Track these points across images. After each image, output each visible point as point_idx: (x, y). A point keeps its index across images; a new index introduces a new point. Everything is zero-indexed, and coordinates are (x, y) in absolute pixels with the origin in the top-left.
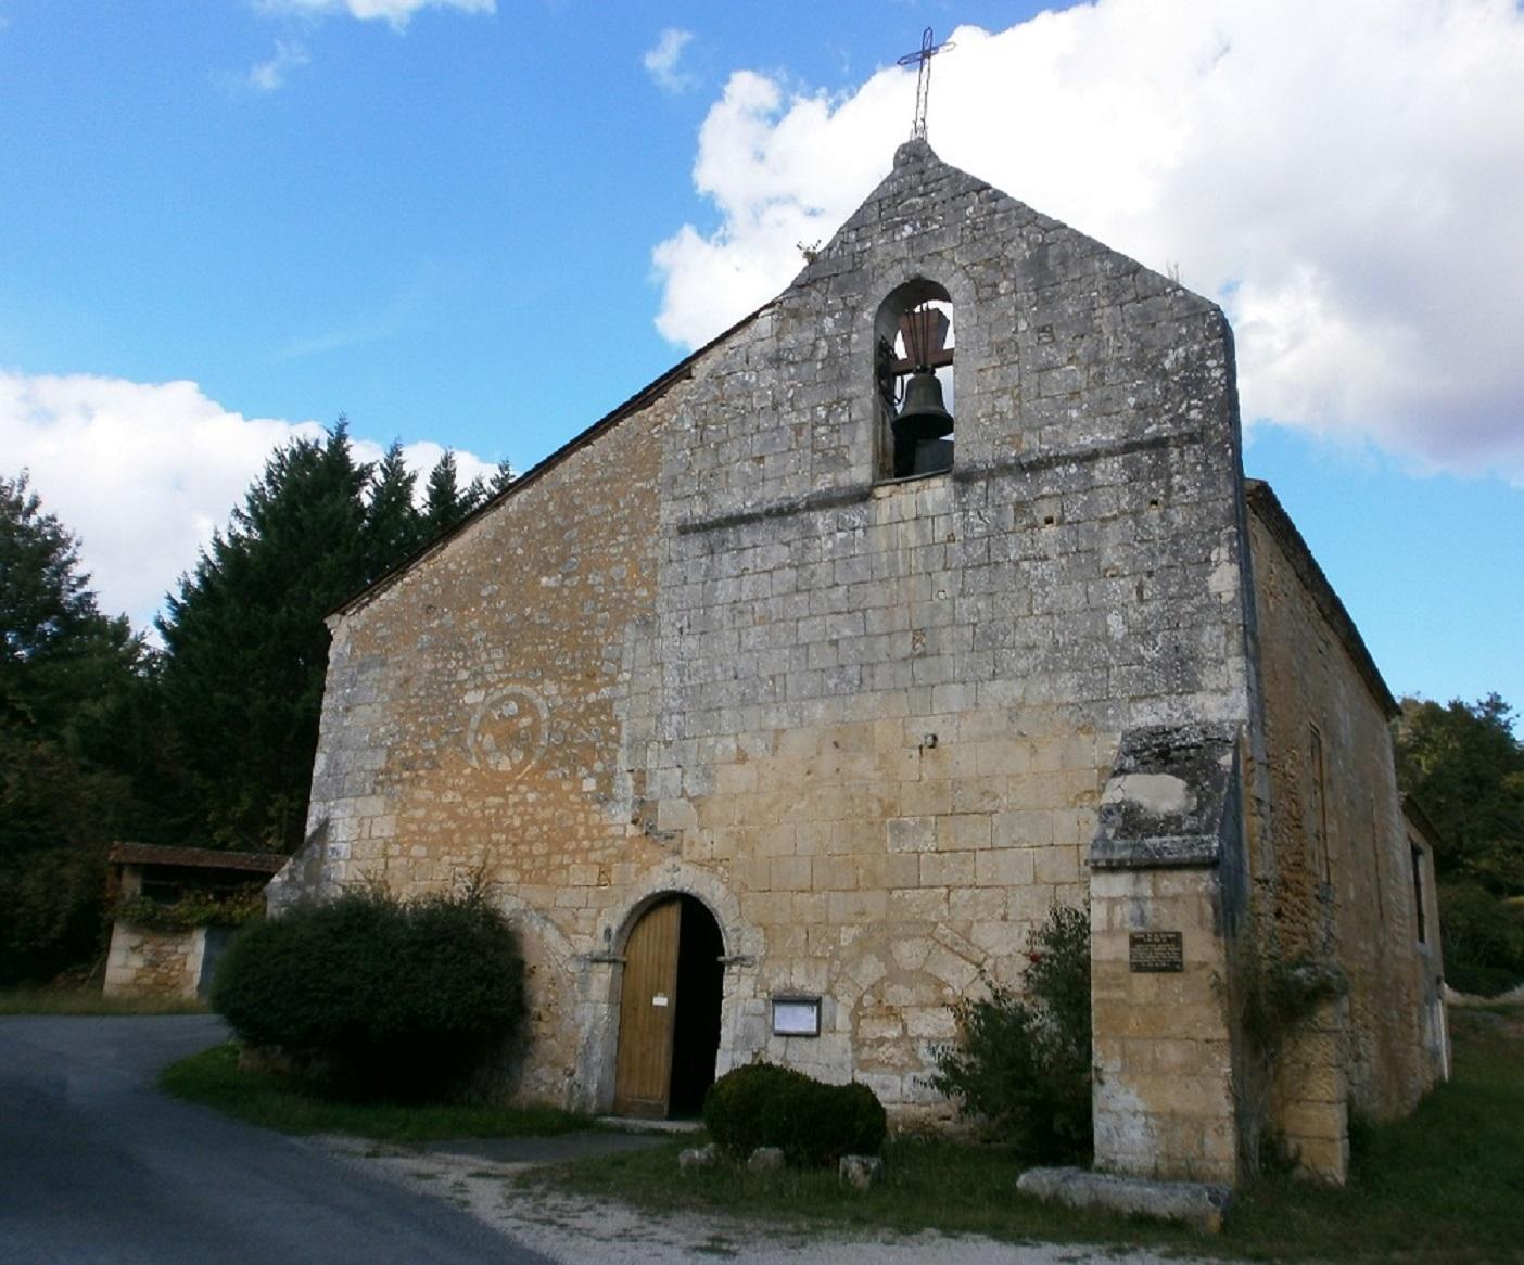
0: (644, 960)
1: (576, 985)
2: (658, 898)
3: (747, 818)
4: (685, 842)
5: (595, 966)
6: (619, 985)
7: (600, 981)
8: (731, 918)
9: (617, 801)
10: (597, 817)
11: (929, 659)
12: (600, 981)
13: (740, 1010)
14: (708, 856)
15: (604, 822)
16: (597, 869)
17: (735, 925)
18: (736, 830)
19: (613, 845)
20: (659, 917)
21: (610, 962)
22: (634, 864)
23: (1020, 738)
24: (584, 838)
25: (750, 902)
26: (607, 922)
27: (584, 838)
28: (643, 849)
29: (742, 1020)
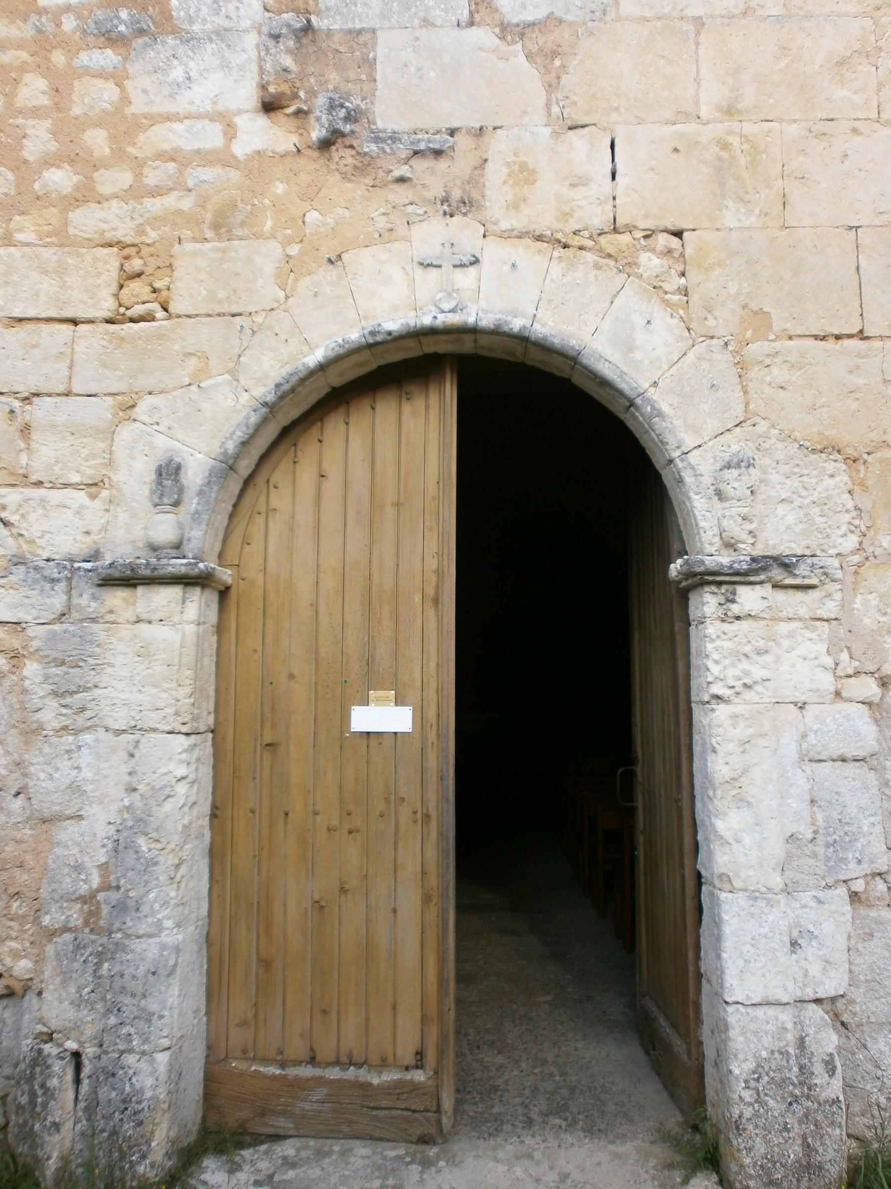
0: (304, 586)
1: (31, 669)
2: (412, 351)
3: (748, 99)
4: (495, 173)
5: (117, 597)
6: (209, 663)
7: (144, 653)
8: (712, 425)
9: (189, 39)
10: (108, 92)
11: (564, 240)
12: (144, 653)
13: (790, 748)
14: (599, 218)
15: (138, 107)
16: (110, 260)
17: (735, 444)
18: (708, 133)
19: (178, 185)
20: (306, 475)
21: (186, 581)
22: (274, 249)
23: (783, 385)
24: (48, 162)
25: (779, 373)
26: (162, 443)
27: (48, 162)
28: (310, 195)
29: (800, 782)
